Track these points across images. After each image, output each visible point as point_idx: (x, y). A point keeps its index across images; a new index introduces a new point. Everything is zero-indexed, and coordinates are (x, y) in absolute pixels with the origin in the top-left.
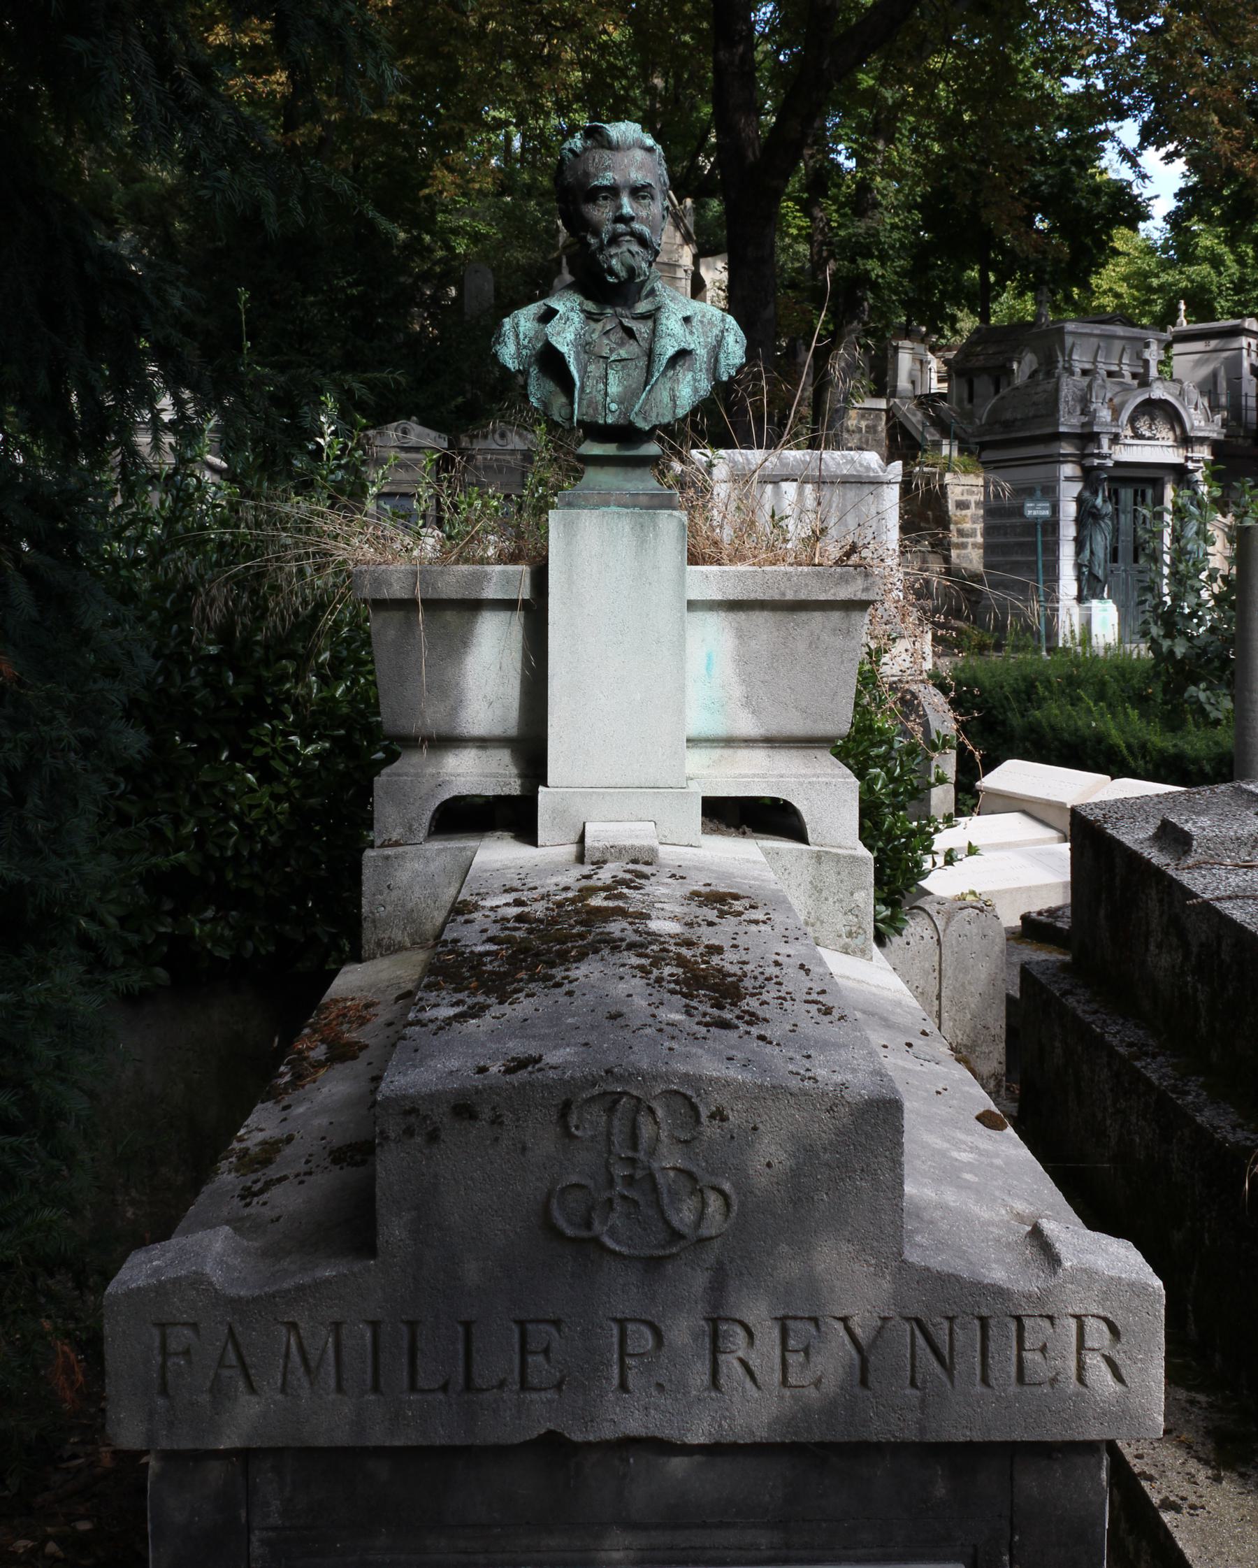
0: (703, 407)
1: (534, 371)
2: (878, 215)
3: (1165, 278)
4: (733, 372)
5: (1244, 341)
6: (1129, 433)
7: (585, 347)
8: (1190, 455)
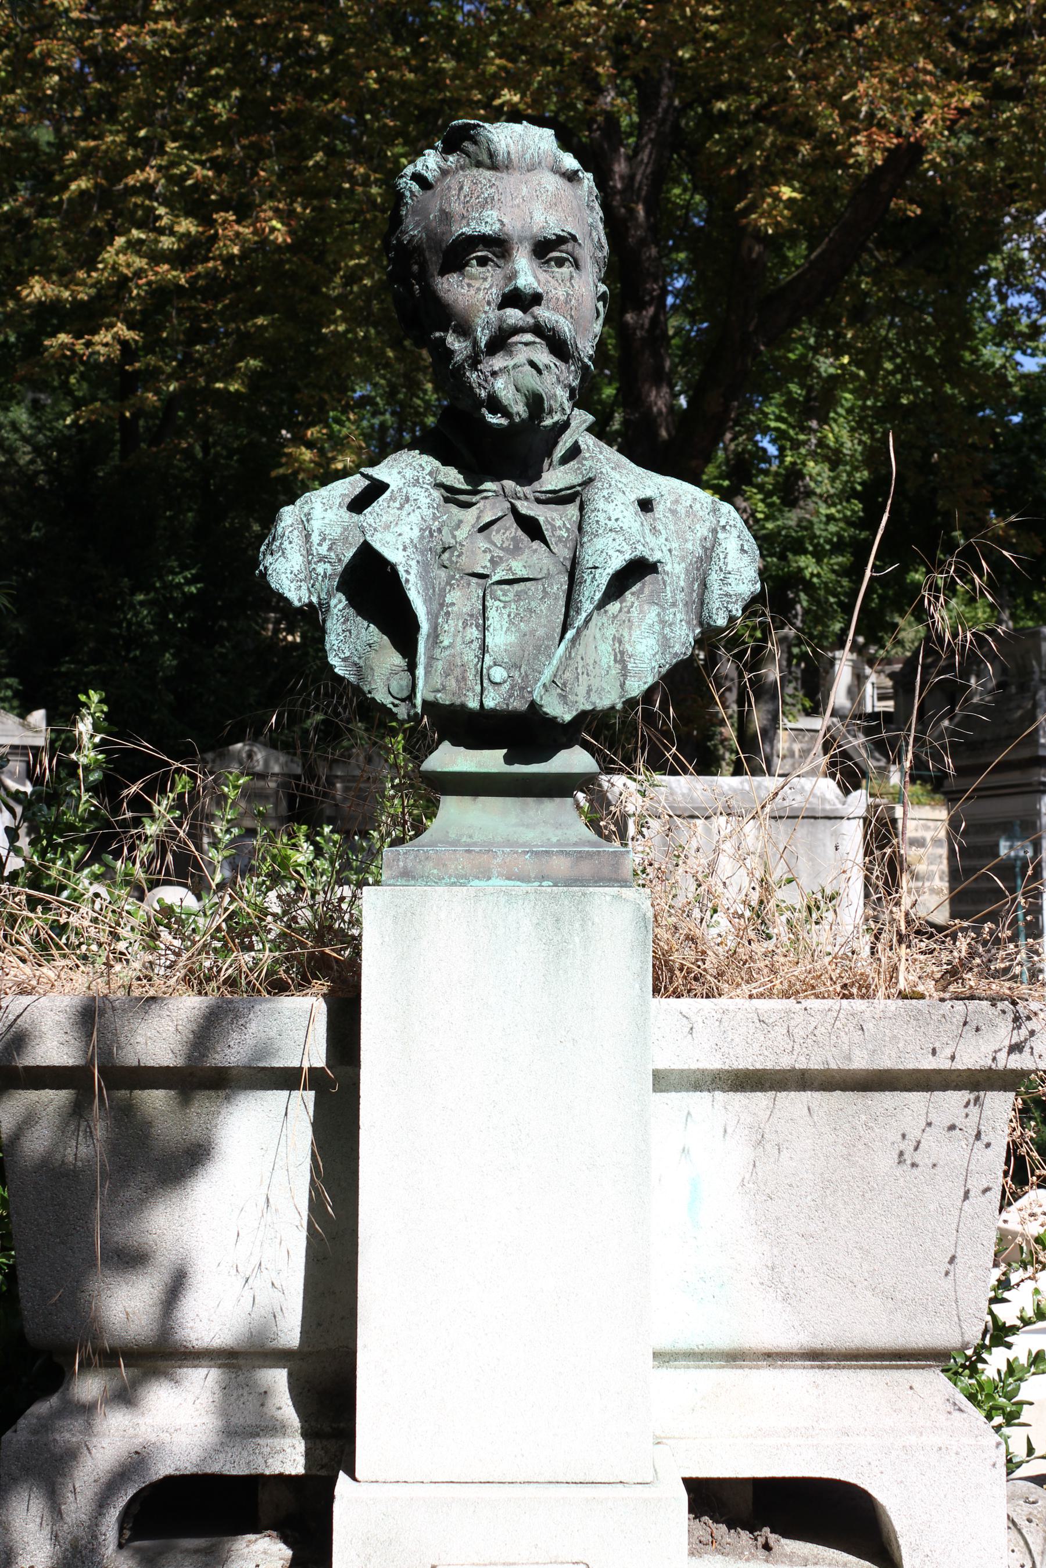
0: (684, 682)
1: (339, 602)
2: (812, 506)
4: (737, 610)
7: (440, 552)
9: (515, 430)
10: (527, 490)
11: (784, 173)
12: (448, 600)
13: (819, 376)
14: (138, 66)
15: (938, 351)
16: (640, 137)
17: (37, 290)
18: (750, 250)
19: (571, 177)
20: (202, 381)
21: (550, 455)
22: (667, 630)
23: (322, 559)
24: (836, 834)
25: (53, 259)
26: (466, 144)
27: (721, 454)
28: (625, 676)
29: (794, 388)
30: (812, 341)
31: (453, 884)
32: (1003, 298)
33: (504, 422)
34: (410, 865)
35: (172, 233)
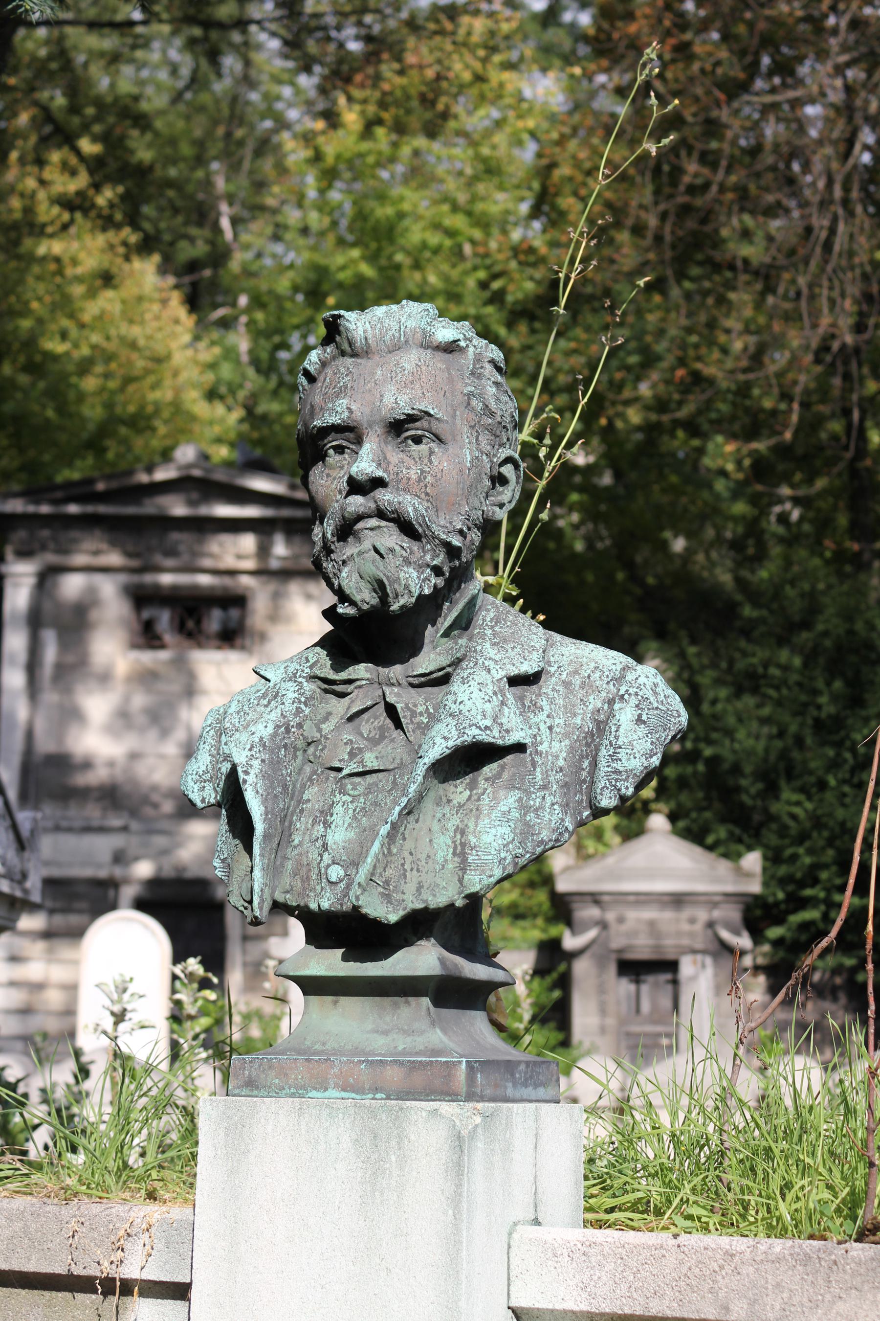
12: (305, 797)
22: (531, 816)
28: (464, 870)
34: (254, 1074)
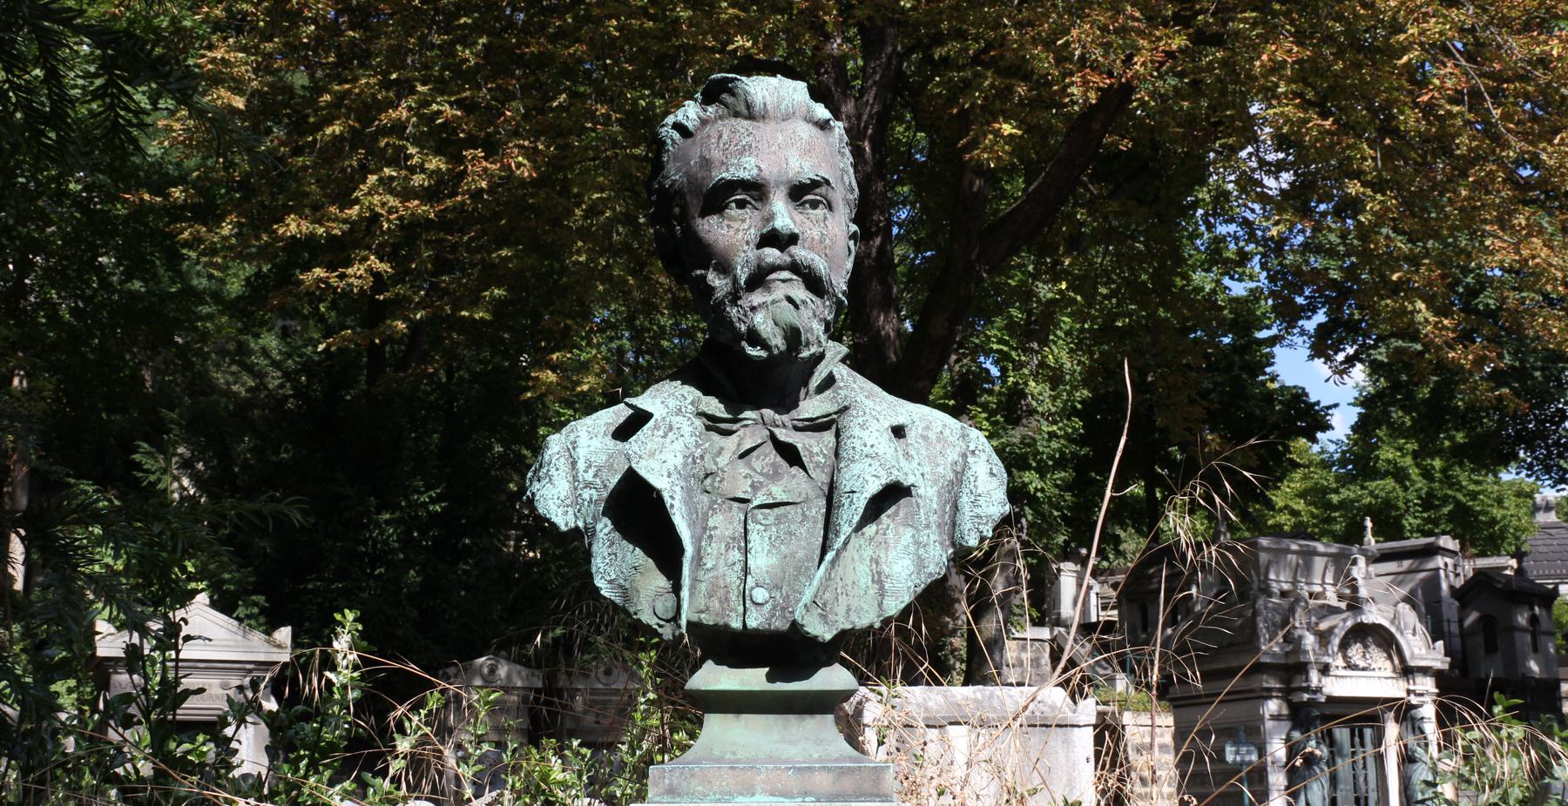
0: (933, 598)
1: (605, 527)
3: (1345, 493)
5: (1439, 561)
6: (1340, 662)
7: (703, 478)
8: (1412, 687)
9: (774, 362)
10: (785, 418)
11: (1003, 112)
13: (1039, 301)
14: (391, 16)
15: (1151, 277)
16: (865, 80)
17: (293, 226)
18: (971, 184)
19: (823, 126)
20: (448, 309)
21: (806, 384)
22: (921, 551)
23: (588, 485)
24: (1067, 742)
25: (307, 194)
26: (724, 96)
27: (946, 376)
28: (882, 595)
29: (1014, 312)
30: (1031, 268)
31: (718, 801)
32: (1210, 227)
33: (763, 354)
34: (675, 782)
35: (423, 170)
